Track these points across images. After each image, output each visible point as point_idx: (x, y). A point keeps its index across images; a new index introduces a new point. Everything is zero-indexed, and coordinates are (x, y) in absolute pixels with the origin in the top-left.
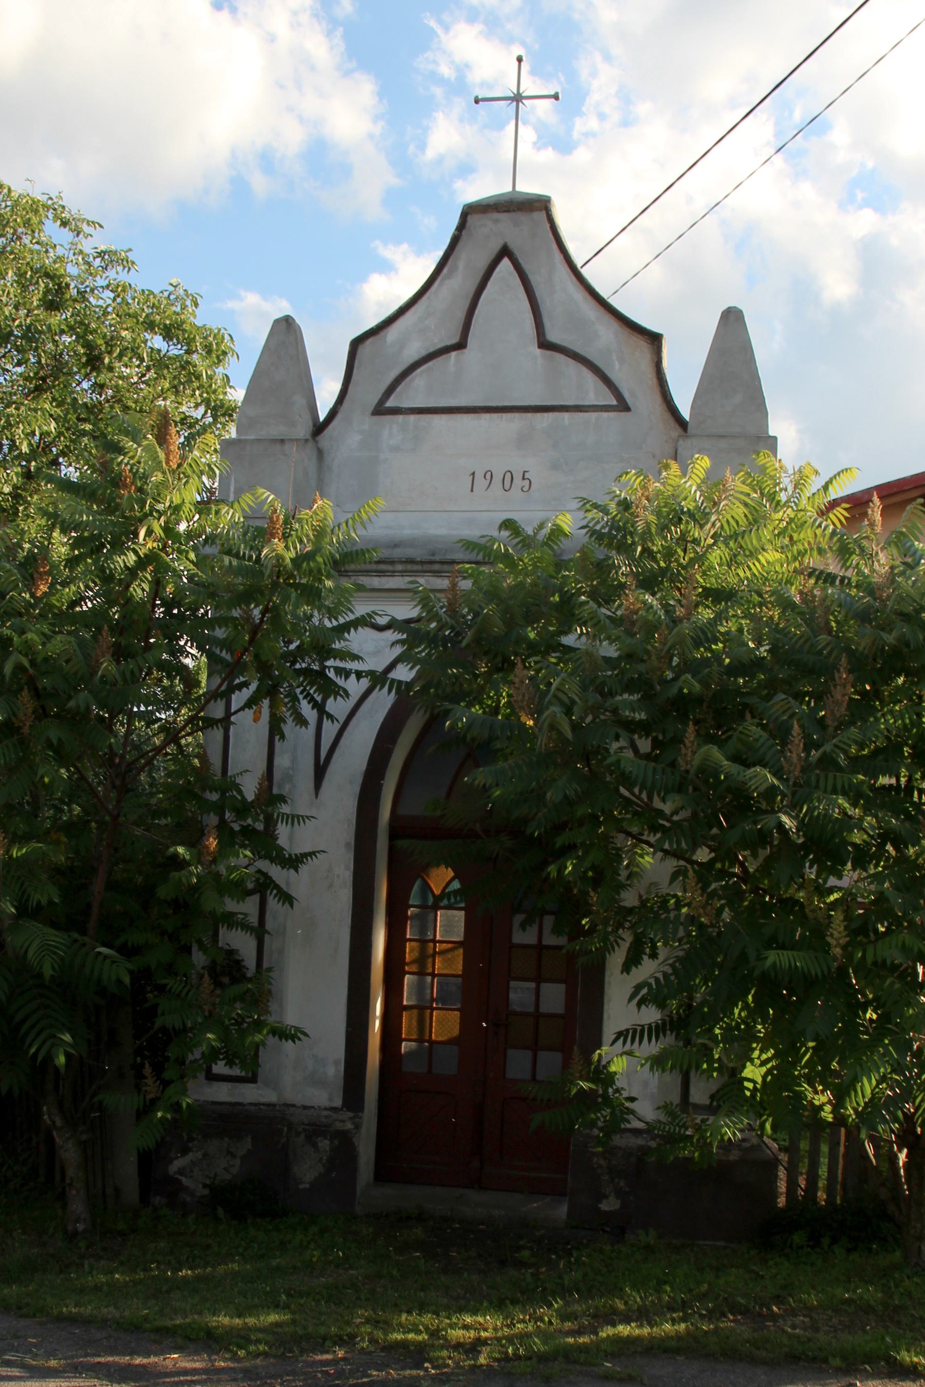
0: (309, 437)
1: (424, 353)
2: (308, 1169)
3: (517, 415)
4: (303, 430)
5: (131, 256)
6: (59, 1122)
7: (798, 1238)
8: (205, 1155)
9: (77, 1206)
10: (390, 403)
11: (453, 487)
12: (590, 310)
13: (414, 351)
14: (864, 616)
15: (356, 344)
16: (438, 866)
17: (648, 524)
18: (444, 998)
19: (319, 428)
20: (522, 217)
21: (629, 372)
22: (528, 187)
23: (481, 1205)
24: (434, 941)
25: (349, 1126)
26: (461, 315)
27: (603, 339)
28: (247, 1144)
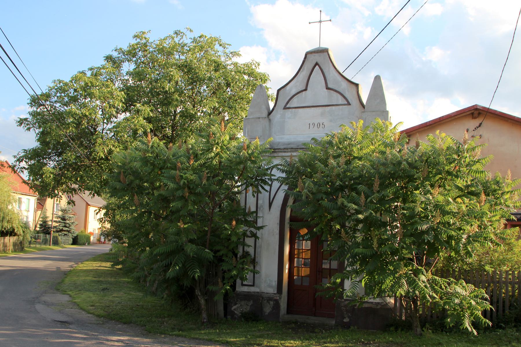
0: (266, 116)
1: (296, 92)
2: (267, 309)
3: (321, 108)
4: (265, 114)
5: (240, 53)
6: (200, 294)
7: (392, 329)
8: (241, 305)
9: (204, 315)
10: (287, 106)
11: (301, 129)
12: (339, 78)
13: (294, 92)
14: (384, 164)
15: (279, 91)
16: (302, 228)
17: (336, 142)
18: (305, 264)
19: (270, 113)
20: (321, 54)
21: (350, 95)
22: (323, 46)
23: (312, 320)
24: (302, 249)
25: (278, 298)
26: (306, 81)
27: (343, 86)
28: (251, 303)
